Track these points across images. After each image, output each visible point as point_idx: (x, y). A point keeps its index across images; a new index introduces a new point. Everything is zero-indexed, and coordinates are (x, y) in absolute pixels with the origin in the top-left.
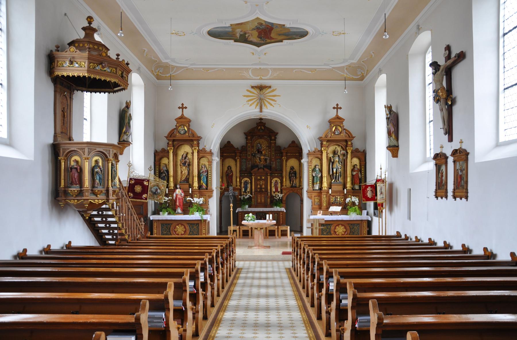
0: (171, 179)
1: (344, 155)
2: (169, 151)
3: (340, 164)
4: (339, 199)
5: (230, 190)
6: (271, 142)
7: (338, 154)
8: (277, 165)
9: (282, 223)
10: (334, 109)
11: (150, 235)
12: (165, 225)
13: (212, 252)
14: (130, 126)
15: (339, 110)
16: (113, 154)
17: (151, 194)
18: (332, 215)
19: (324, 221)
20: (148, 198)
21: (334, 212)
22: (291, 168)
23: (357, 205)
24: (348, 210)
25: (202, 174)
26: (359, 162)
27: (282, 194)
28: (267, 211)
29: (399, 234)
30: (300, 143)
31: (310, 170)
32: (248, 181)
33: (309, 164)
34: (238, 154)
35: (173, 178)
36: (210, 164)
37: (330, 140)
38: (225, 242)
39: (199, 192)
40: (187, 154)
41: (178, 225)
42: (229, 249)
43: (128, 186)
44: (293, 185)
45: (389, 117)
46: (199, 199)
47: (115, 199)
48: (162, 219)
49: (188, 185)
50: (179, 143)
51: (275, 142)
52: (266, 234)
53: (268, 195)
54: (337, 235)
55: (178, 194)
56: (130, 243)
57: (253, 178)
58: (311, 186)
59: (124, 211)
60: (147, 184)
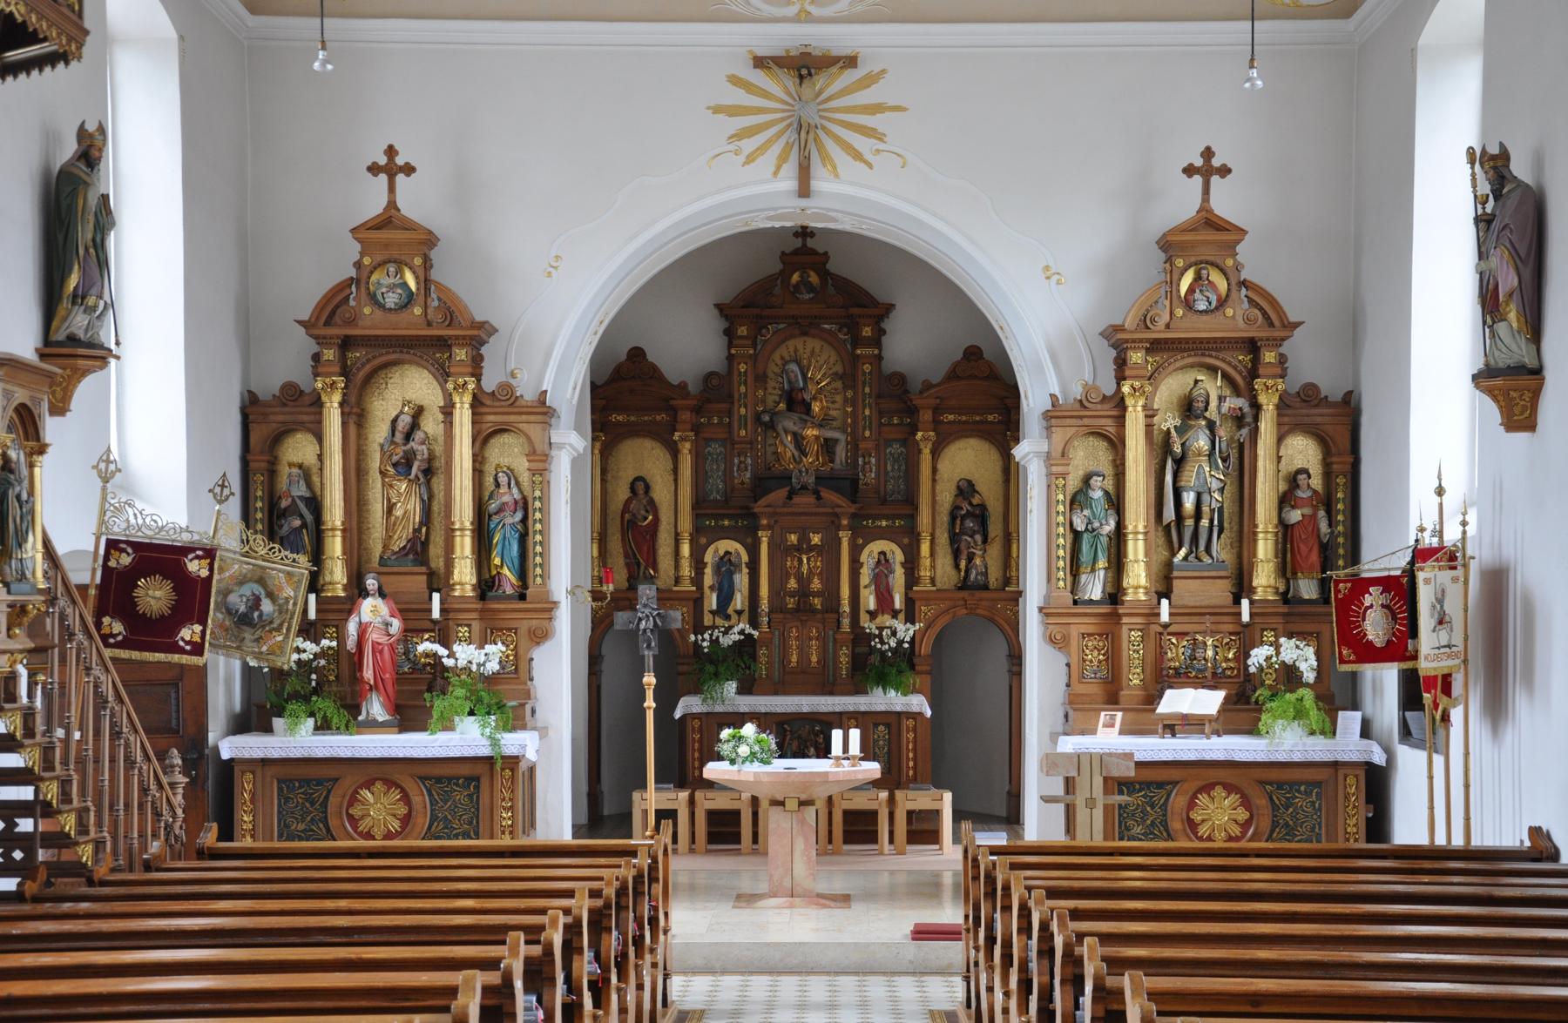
0: (335, 546)
1: (1238, 420)
2: (324, 398)
3: (1217, 468)
4: (1210, 653)
5: (644, 600)
6: (859, 352)
7: (1207, 414)
8: (886, 473)
9: (915, 773)
10: (1190, 176)
11: (219, 839)
12: (300, 787)
13: (542, 928)
14: (103, 263)
15: (1215, 179)
16: (10, 412)
17: (227, 623)
18: (1174, 735)
19: (1133, 765)
20: (207, 645)
21: (1185, 717)
22: (958, 487)
23: (1308, 685)
24: (1260, 711)
25: (496, 519)
26: (1320, 457)
27: (913, 623)
28: (834, 713)
29: (1543, 843)
30: (1008, 358)
31: (1061, 497)
32: (738, 554)
33: (1055, 469)
34: (685, 416)
35: (344, 538)
36: (540, 466)
37: (1166, 341)
38: (616, 870)
39: (482, 611)
40: (419, 412)
41: (368, 785)
42: (634, 911)
43: (98, 580)
44: (972, 577)
45: (1493, 215)
46: (483, 652)
47: (21, 651)
48: (284, 755)
49: (425, 577)
50: (374, 357)
51: (876, 352)
52: (830, 832)
53: (839, 627)
54: (1200, 839)
55: (368, 624)
56: (103, 883)
57: (765, 539)
58: (1061, 584)
59: (74, 713)
60: (204, 573)
